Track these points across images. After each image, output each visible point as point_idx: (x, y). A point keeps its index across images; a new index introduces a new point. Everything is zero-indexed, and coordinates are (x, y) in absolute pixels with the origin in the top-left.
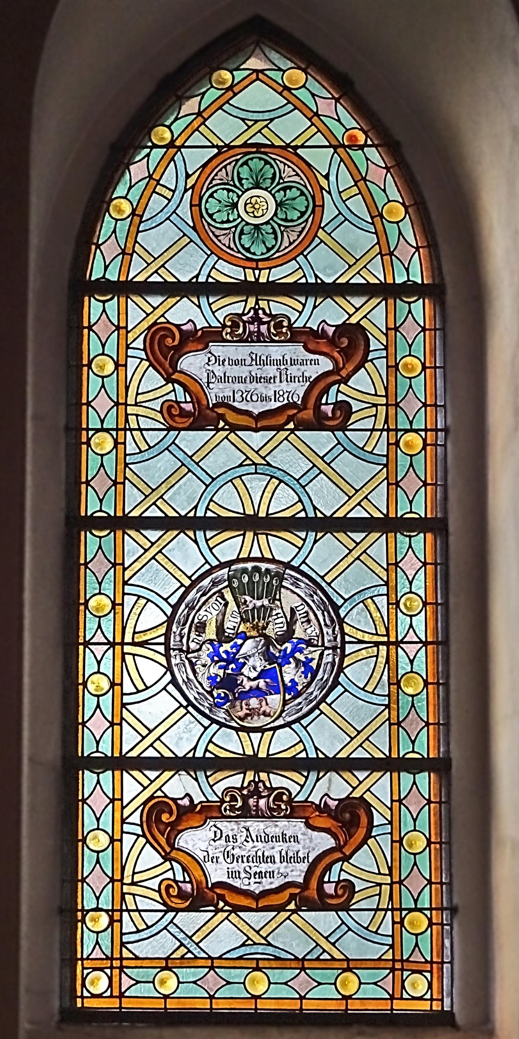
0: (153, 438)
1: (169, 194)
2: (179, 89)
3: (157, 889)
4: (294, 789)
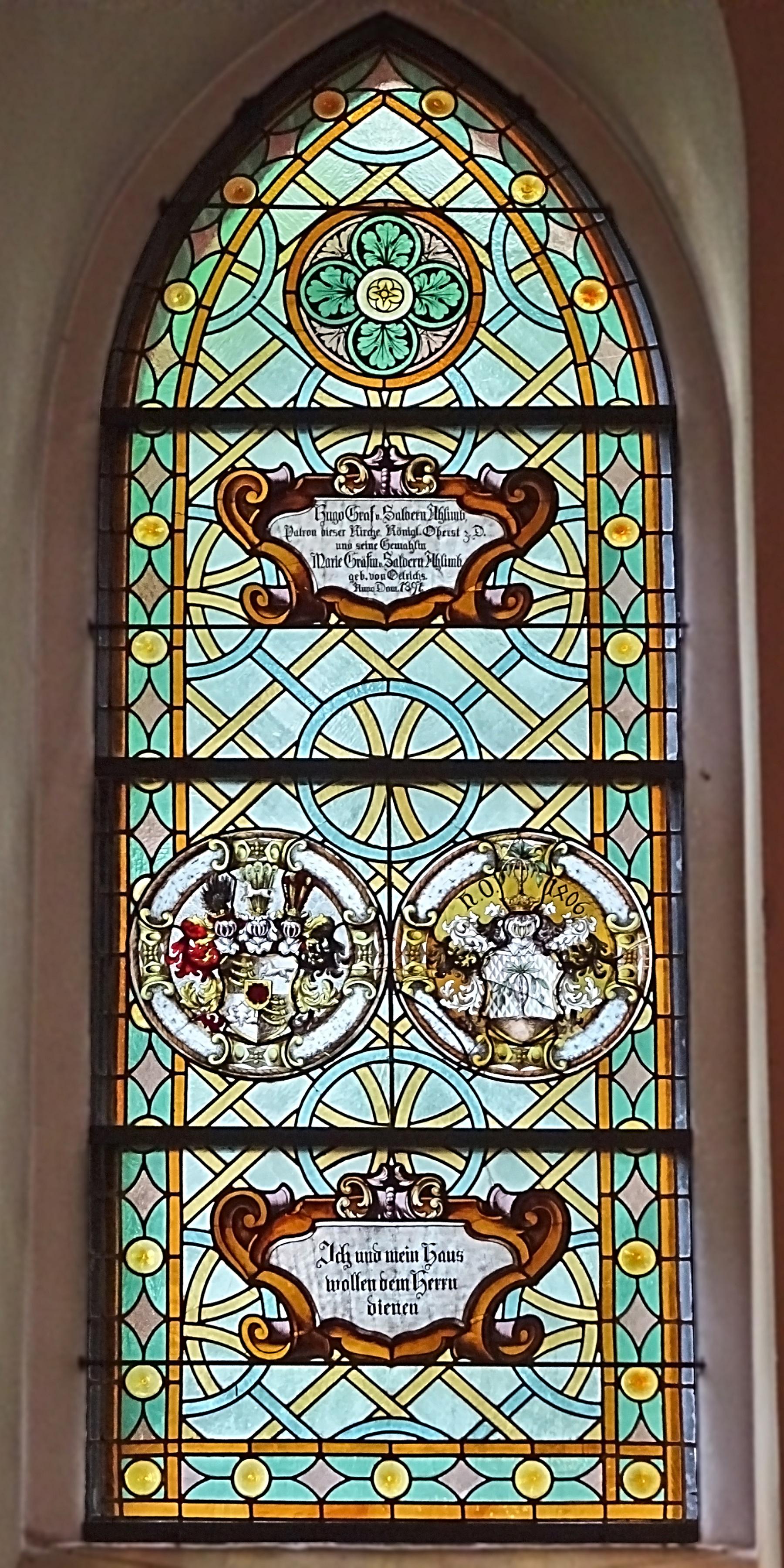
0: (226, 1375)
1: (252, 277)
2: (265, 123)
3: (237, 1332)
4: (442, 457)
